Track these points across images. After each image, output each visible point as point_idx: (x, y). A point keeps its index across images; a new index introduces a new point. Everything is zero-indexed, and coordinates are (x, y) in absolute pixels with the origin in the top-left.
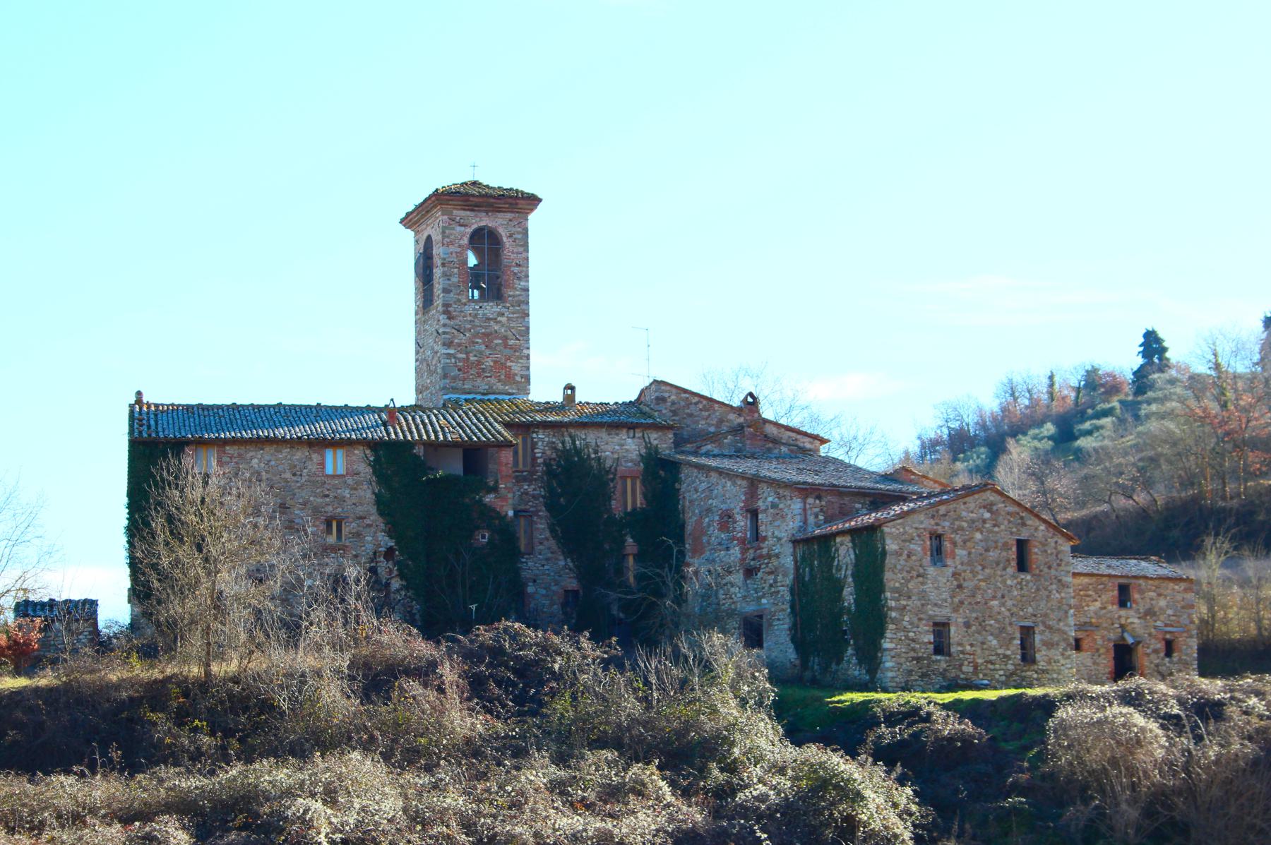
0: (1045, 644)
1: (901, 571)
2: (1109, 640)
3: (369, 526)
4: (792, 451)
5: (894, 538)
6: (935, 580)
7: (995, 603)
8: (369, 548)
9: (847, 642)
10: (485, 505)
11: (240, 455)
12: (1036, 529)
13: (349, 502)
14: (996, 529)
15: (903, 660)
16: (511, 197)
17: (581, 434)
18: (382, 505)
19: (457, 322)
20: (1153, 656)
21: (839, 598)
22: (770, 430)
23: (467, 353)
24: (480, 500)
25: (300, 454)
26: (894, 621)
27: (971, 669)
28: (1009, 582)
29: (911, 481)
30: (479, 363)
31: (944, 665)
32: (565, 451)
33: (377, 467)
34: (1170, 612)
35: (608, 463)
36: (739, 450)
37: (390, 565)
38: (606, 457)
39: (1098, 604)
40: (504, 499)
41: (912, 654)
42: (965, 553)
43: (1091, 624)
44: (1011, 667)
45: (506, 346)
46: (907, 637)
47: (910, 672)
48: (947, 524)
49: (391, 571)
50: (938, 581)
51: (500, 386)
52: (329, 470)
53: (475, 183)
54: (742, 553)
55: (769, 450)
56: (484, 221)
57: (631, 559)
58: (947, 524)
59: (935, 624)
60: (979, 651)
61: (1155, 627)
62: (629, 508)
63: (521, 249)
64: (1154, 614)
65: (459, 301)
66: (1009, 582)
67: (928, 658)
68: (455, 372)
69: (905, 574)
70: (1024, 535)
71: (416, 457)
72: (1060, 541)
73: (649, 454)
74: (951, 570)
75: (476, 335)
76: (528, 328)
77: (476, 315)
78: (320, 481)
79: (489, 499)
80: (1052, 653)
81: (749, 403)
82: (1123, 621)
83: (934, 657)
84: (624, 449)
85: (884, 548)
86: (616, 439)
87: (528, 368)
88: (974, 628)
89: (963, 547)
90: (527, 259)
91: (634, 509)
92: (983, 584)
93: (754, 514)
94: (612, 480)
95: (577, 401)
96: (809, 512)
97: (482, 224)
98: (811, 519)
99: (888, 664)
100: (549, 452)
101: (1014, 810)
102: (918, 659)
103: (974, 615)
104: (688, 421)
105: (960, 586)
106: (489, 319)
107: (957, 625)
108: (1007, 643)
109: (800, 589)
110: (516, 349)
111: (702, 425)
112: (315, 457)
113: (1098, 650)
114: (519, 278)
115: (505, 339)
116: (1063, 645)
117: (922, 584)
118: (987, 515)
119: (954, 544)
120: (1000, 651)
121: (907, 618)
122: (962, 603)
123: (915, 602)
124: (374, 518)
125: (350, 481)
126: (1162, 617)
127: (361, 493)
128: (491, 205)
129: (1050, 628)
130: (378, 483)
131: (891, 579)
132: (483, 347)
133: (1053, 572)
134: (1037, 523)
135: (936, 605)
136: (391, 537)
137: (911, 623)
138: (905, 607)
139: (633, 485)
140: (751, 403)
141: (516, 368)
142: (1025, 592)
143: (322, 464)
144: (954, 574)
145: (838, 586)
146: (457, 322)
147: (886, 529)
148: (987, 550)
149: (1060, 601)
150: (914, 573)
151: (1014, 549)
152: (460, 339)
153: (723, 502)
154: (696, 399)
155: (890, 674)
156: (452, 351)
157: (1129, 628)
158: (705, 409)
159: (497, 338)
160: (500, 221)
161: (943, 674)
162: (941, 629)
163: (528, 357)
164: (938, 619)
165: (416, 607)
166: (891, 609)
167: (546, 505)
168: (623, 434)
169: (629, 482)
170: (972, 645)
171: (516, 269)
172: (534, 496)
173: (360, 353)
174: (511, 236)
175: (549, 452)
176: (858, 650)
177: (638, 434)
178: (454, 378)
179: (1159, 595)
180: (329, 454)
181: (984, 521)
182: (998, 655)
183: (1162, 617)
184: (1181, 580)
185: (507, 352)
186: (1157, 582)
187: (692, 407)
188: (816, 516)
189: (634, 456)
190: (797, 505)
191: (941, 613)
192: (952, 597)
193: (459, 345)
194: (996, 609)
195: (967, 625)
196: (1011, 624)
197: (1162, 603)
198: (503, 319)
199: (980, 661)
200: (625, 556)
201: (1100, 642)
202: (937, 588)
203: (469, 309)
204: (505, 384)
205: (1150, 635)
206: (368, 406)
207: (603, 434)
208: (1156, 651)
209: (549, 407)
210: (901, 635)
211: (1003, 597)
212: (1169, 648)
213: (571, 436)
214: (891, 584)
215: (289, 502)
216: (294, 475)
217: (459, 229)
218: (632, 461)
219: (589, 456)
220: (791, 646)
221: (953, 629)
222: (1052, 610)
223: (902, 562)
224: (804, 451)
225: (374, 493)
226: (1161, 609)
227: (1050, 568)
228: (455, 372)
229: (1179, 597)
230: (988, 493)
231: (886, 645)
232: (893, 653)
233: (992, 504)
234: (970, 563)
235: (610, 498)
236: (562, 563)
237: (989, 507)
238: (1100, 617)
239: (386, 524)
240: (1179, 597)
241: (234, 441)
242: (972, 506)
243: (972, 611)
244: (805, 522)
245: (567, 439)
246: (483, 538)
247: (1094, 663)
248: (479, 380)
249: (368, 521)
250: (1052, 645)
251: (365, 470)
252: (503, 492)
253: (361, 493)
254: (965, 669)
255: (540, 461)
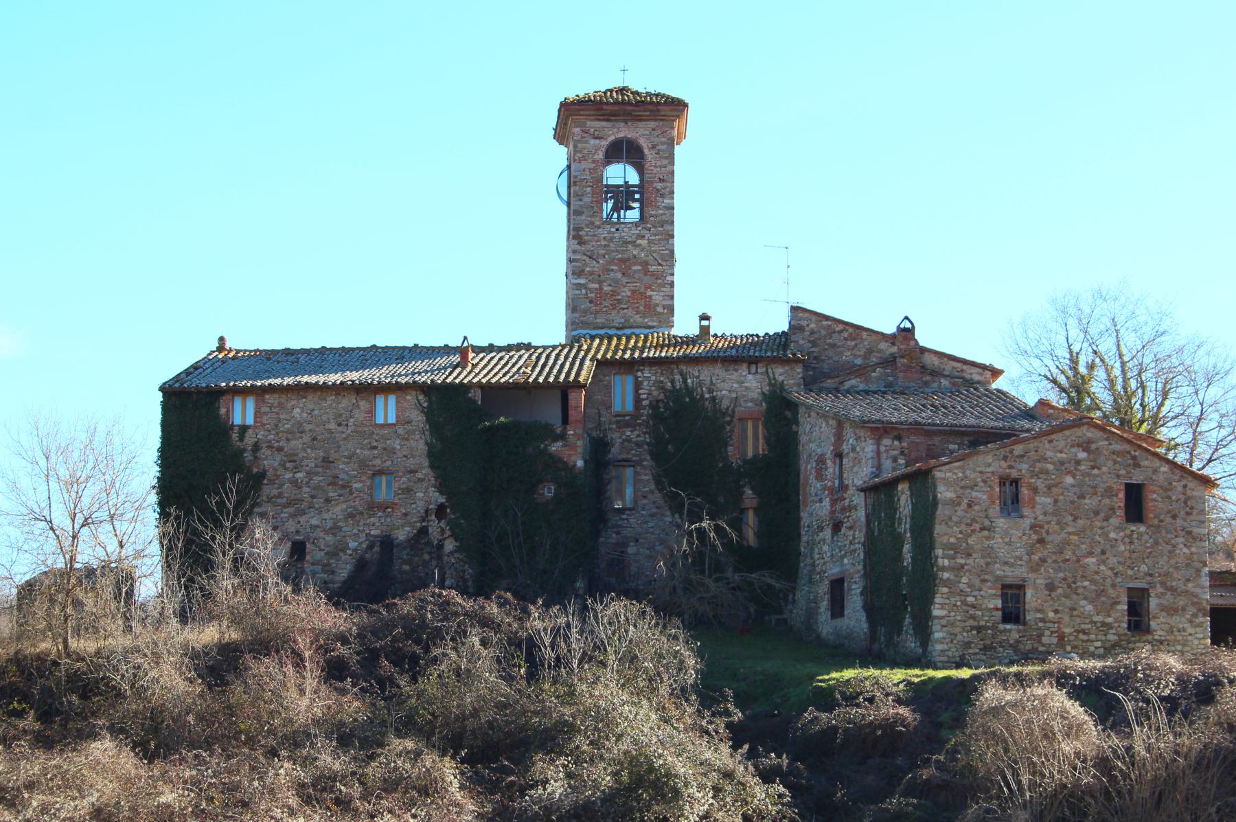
0: (1164, 608)
1: (958, 523)
4: (954, 384)
5: (949, 484)
6: (1006, 533)
7: (1091, 561)
8: (421, 505)
9: (906, 607)
10: (551, 455)
11: (280, 404)
12: (1155, 471)
13: (400, 454)
14: (1096, 471)
15: (957, 630)
16: (652, 103)
17: (694, 370)
18: (436, 458)
19: (589, 247)
21: (899, 557)
22: (929, 360)
23: (600, 283)
24: (546, 449)
25: (346, 402)
26: (946, 583)
27: (1055, 641)
28: (1112, 535)
29: (1049, 416)
33: (429, 414)
36: (889, 385)
38: (722, 398)
40: (574, 447)
41: (971, 622)
42: (1049, 500)
44: (1112, 638)
45: (646, 272)
46: (964, 603)
47: (967, 645)
48: (1024, 467)
49: (443, 531)
51: (638, 319)
52: (380, 420)
53: (622, 90)
54: (832, 505)
55: (926, 384)
56: (624, 131)
57: (751, 513)
58: (1024, 467)
59: (1004, 587)
60: (1066, 618)
62: (750, 454)
63: (665, 162)
65: (592, 223)
67: (994, 627)
68: (585, 305)
69: (963, 527)
70: (1137, 478)
72: (1190, 485)
73: (773, 392)
74: (1027, 522)
75: (611, 262)
76: (672, 252)
77: (611, 240)
78: (369, 431)
80: (1175, 620)
81: (905, 330)
83: (1001, 627)
84: (745, 387)
85: (935, 497)
86: (735, 376)
87: (672, 297)
88: (1060, 591)
89: (1047, 494)
90: (673, 173)
91: (755, 456)
93: (839, 455)
94: (729, 423)
95: (712, 333)
96: (884, 456)
97: (621, 135)
100: (655, 393)
102: (979, 629)
103: (1061, 575)
104: (830, 353)
105: (1041, 541)
106: (627, 243)
107: (1035, 588)
111: (846, 356)
112: (363, 404)
115: (645, 264)
116: (1192, 610)
117: (988, 538)
118: (1082, 455)
119: (1035, 490)
120: (1096, 619)
121: (964, 580)
122: (1043, 560)
123: (977, 560)
124: (426, 472)
125: (401, 431)
128: (629, 114)
129: (1173, 590)
130: (431, 434)
132: (619, 275)
133: (1179, 522)
134: (1157, 463)
135: (1006, 563)
136: (441, 493)
137: (970, 585)
138: (962, 566)
139: (755, 428)
140: (906, 333)
141: (657, 297)
143: (372, 412)
144: (1032, 527)
145: (898, 540)
146: (589, 247)
147: (938, 474)
148: (1082, 497)
149: (1190, 557)
150: (977, 526)
151: (1122, 495)
152: (592, 266)
153: (819, 446)
154: (841, 327)
155: (939, 647)
156: (582, 281)
159: (635, 264)
160: (641, 131)
161: (1015, 647)
162: (1012, 596)
163: (672, 284)
164: (1009, 581)
165: (469, 571)
166: (943, 569)
167: (651, 454)
168: (743, 369)
169: (750, 424)
170: (1056, 612)
171: (659, 185)
172: (637, 444)
173: (491, 286)
174: (653, 147)
175: (655, 393)
176: (913, 617)
178: (585, 312)
180: (380, 400)
181: (1078, 462)
182: (1092, 622)
185: (647, 279)
187: (836, 336)
188: (895, 460)
190: (869, 447)
191: (1013, 574)
192: (1030, 554)
193: (591, 273)
194: (1093, 568)
195: (1051, 587)
196: (1114, 586)
198: (644, 242)
199: (1067, 630)
200: (743, 511)
202: (1009, 544)
203: (603, 232)
204: (644, 317)
206: (446, 346)
207: (719, 370)
209: (688, 341)
213: (681, 374)
215: (333, 456)
216: (340, 425)
217: (592, 142)
218: (752, 400)
219: (702, 396)
220: (864, 614)
221: (1029, 593)
222: (1177, 568)
223: (959, 513)
224: (970, 383)
225: (427, 443)
227: (1174, 517)
228: (585, 305)
231: (937, 612)
232: (944, 622)
233: (1090, 442)
234: (1056, 513)
235: (726, 445)
236: (669, 519)
237: (1086, 445)
239: (436, 478)
241: (272, 389)
244: (879, 467)
245: (677, 377)
248: (614, 313)
249: (419, 475)
250: (1176, 610)
251: (418, 418)
252: (572, 439)
253: (413, 443)
254: (1045, 640)
255: (645, 403)
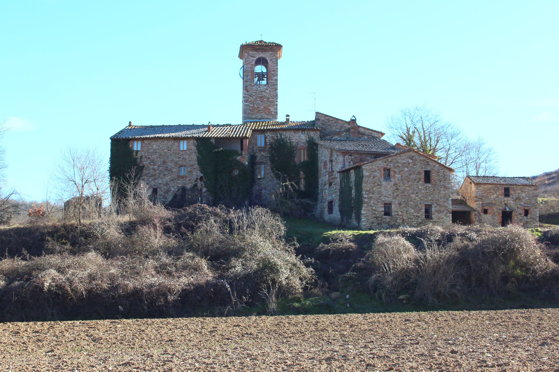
2: (500, 210)
3: (195, 169)
4: (369, 138)
5: (367, 170)
11: (149, 144)
12: (434, 166)
15: (369, 218)
17: (284, 133)
18: (200, 162)
20: (519, 216)
21: (351, 194)
22: (360, 130)
23: (254, 104)
25: (170, 143)
26: (366, 203)
27: (401, 221)
28: (420, 187)
29: (400, 148)
30: (258, 108)
31: (388, 220)
32: (277, 139)
33: (198, 147)
34: (527, 198)
35: (294, 144)
36: (348, 138)
37: (202, 183)
39: (495, 196)
41: (374, 216)
42: (400, 176)
43: (492, 203)
44: (420, 221)
45: (268, 101)
46: (372, 209)
47: (373, 223)
49: (202, 185)
50: (387, 188)
51: (266, 116)
53: (261, 41)
59: (385, 204)
60: (405, 214)
61: (520, 205)
64: (520, 199)
66: (420, 187)
67: (381, 217)
69: (372, 184)
70: (428, 169)
71: (211, 143)
73: (310, 140)
74: (393, 183)
75: (257, 97)
78: (178, 152)
80: (440, 215)
82: (506, 202)
83: (384, 217)
84: (301, 138)
86: (297, 135)
89: (399, 174)
90: (277, 68)
92: (408, 188)
98: (347, 164)
99: (363, 220)
101: (350, 278)
102: (377, 218)
104: (329, 127)
105: (397, 189)
107: (395, 204)
109: (342, 191)
110: (272, 102)
111: (334, 129)
112: (176, 144)
113: (494, 214)
114: (274, 76)
115: (268, 98)
116: (446, 212)
117: (380, 188)
118: (411, 161)
119: (395, 172)
121: (372, 202)
122: (398, 195)
123: (376, 195)
124: (196, 166)
125: (188, 152)
126: (523, 201)
127: (192, 157)
128: (263, 49)
129: (439, 205)
131: (365, 186)
133: (442, 183)
134: (435, 164)
137: (373, 203)
138: (371, 197)
139: (304, 152)
140: (353, 121)
141: (272, 109)
142: (428, 191)
143: (179, 146)
144: (394, 184)
145: (351, 189)
147: (363, 167)
148: (410, 175)
149: (445, 195)
150: (376, 184)
151: (423, 174)
152: (251, 99)
154: (332, 119)
155: (364, 223)
156: (248, 104)
157: (509, 205)
158: (335, 123)
163: (277, 105)
164: (386, 202)
166: (365, 198)
168: (300, 133)
170: (402, 212)
171: (273, 73)
172: (265, 157)
176: (355, 214)
177: (306, 133)
178: (249, 114)
179: (522, 192)
180: (181, 142)
181: (409, 163)
183: (523, 201)
184: (532, 185)
185: (269, 103)
186: (521, 187)
187: (330, 122)
188: (349, 162)
189: (304, 141)
191: (388, 200)
192: (393, 193)
193: (251, 101)
195: (400, 204)
196: (420, 204)
197: (524, 195)
198: (268, 91)
199: (405, 218)
201: (495, 210)
203: (254, 88)
205: (518, 207)
207: (292, 133)
208: (520, 214)
209: (282, 123)
210: (369, 208)
211: (417, 193)
214: (366, 188)
217: (251, 58)
221: (393, 206)
224: (374, 138)
226: (523, 197)
229: (531, 193)
230: (411, 152)
231: (363, 212)
233: (413, 157)
234: (402, 180)
235: (294, 157)
237: (412, 158)
238: (496, 201)
240: (531, 193)
241: (146, 139)
242: (404, 157)
243: (403, 198)
244: (344, 165)
245: (279, 135)
247: (493, 219)
250: (440, 212)
251: (194, 148)
252: (244, 155)
253: (192, 157)
254: (398, 221)
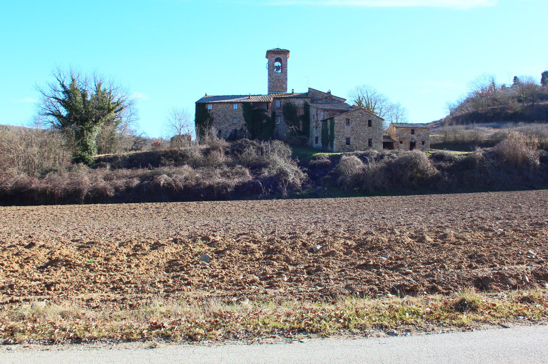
18: (245, 115)
25: (228, 105)
50: (347, 130)
53: (278, 49)
56: (278, 56)
79: (266, 113)
84: (300, 103)
93: (317, 115)
101: (327, 179)
108: (365, 142)
111: (318, 97)
124: (243, 118)
140: (329, 93)
141: (284, 86)
143: (233, 107)
145: (328, 130)
165: (250, 135)
189: (302, 104)
190: (322, 113)
191: (348, 136)
195: (355, 138)
197: (422, 133)
207: (295, 99)
209: (290, 94)
212: (423, 143)
224: (341, 102)
237: (361, 113)
246: (265, 121)
251: (241, 108)
